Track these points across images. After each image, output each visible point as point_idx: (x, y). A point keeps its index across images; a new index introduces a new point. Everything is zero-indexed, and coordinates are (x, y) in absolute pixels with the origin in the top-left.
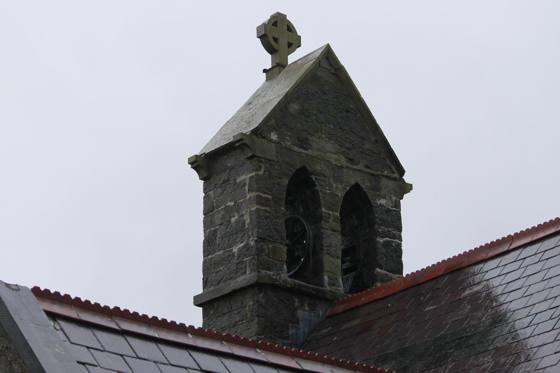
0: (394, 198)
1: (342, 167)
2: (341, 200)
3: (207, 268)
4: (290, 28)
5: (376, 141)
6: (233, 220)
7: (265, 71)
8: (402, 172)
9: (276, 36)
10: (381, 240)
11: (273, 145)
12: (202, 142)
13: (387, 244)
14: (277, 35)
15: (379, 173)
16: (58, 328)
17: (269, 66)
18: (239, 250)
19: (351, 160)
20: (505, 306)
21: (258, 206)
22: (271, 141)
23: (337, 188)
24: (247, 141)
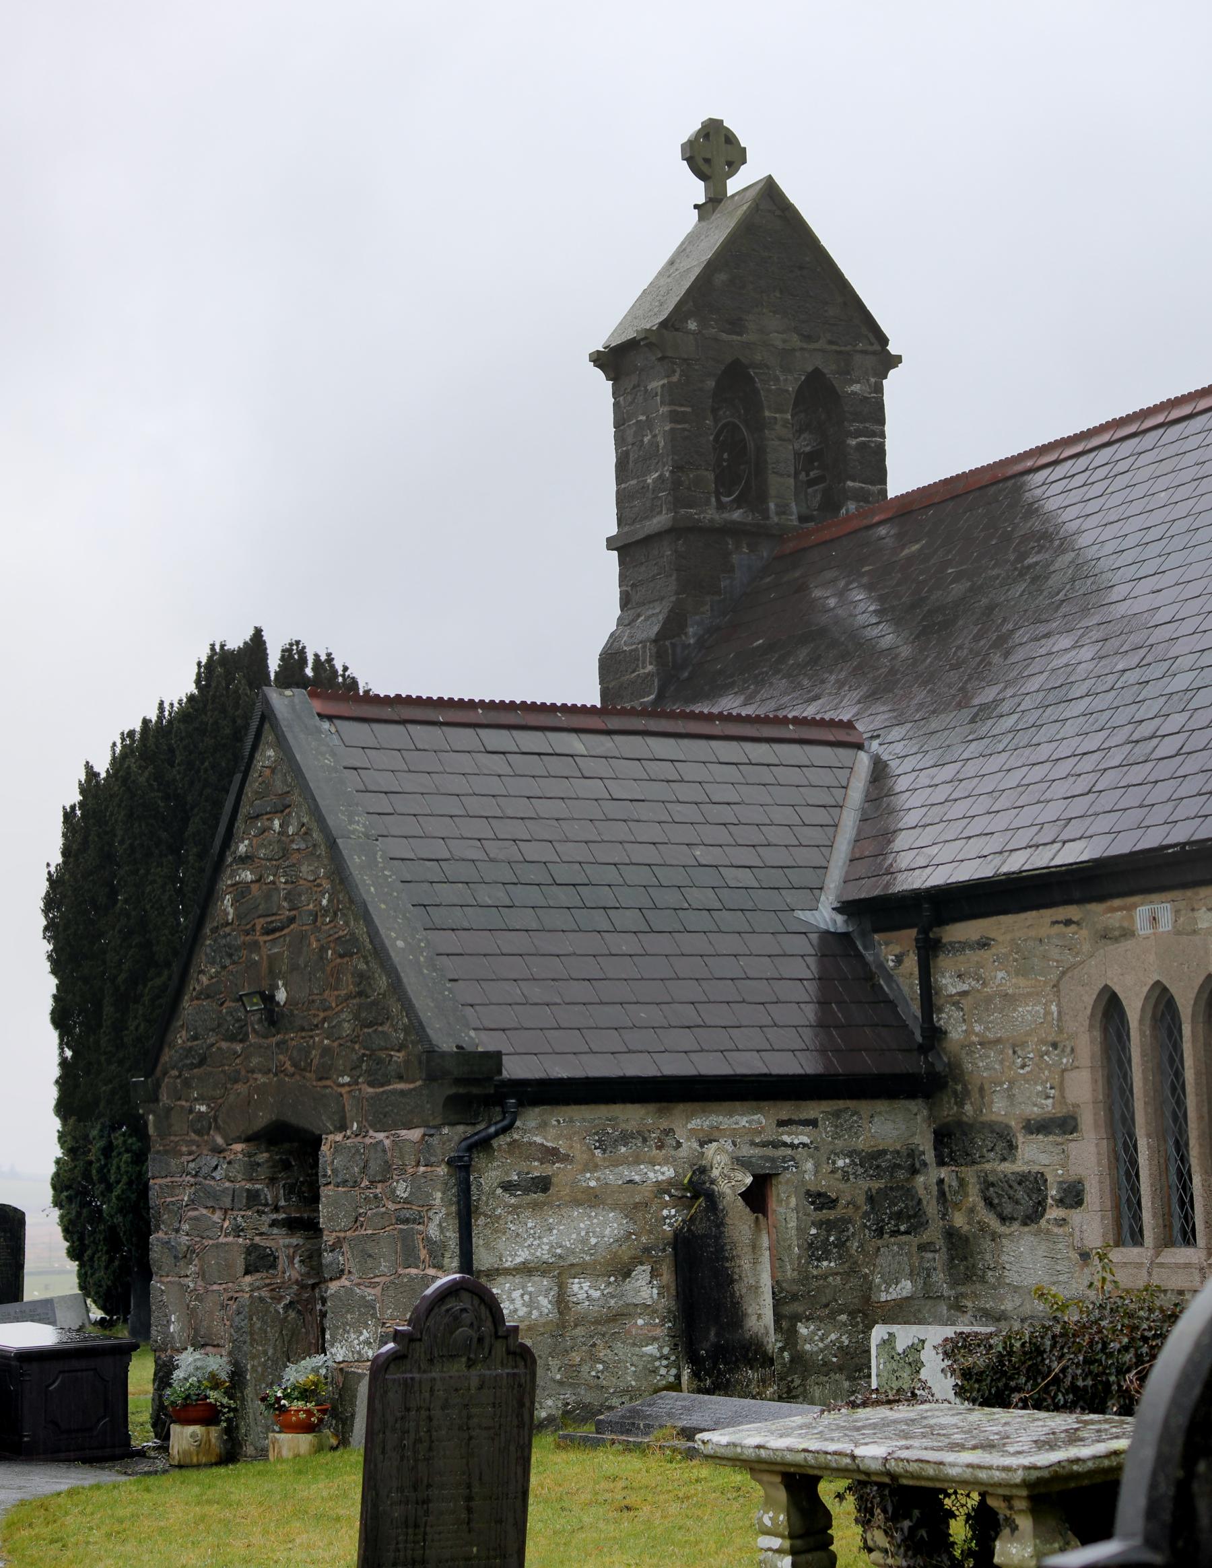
0: (873, 380)
1: (794, 350)
2: (793, 396)
3: (623, 499)
4: (730, 139)
5: (845, 304)
6: (646, 440)
7: (696, 207)
8: (883, 340)
9: (709, 156)
10: (853, 442)
11: (691, 337)
13: (863, 445)
14: (712, 151)
15: (849, 348)
16: (333, 730)
17: (701, 200)
18: (655, 481)
19: (808, 338)
21: (673, 425)
22: (689, 332)
23: (786, 380)
24: (653, 339)
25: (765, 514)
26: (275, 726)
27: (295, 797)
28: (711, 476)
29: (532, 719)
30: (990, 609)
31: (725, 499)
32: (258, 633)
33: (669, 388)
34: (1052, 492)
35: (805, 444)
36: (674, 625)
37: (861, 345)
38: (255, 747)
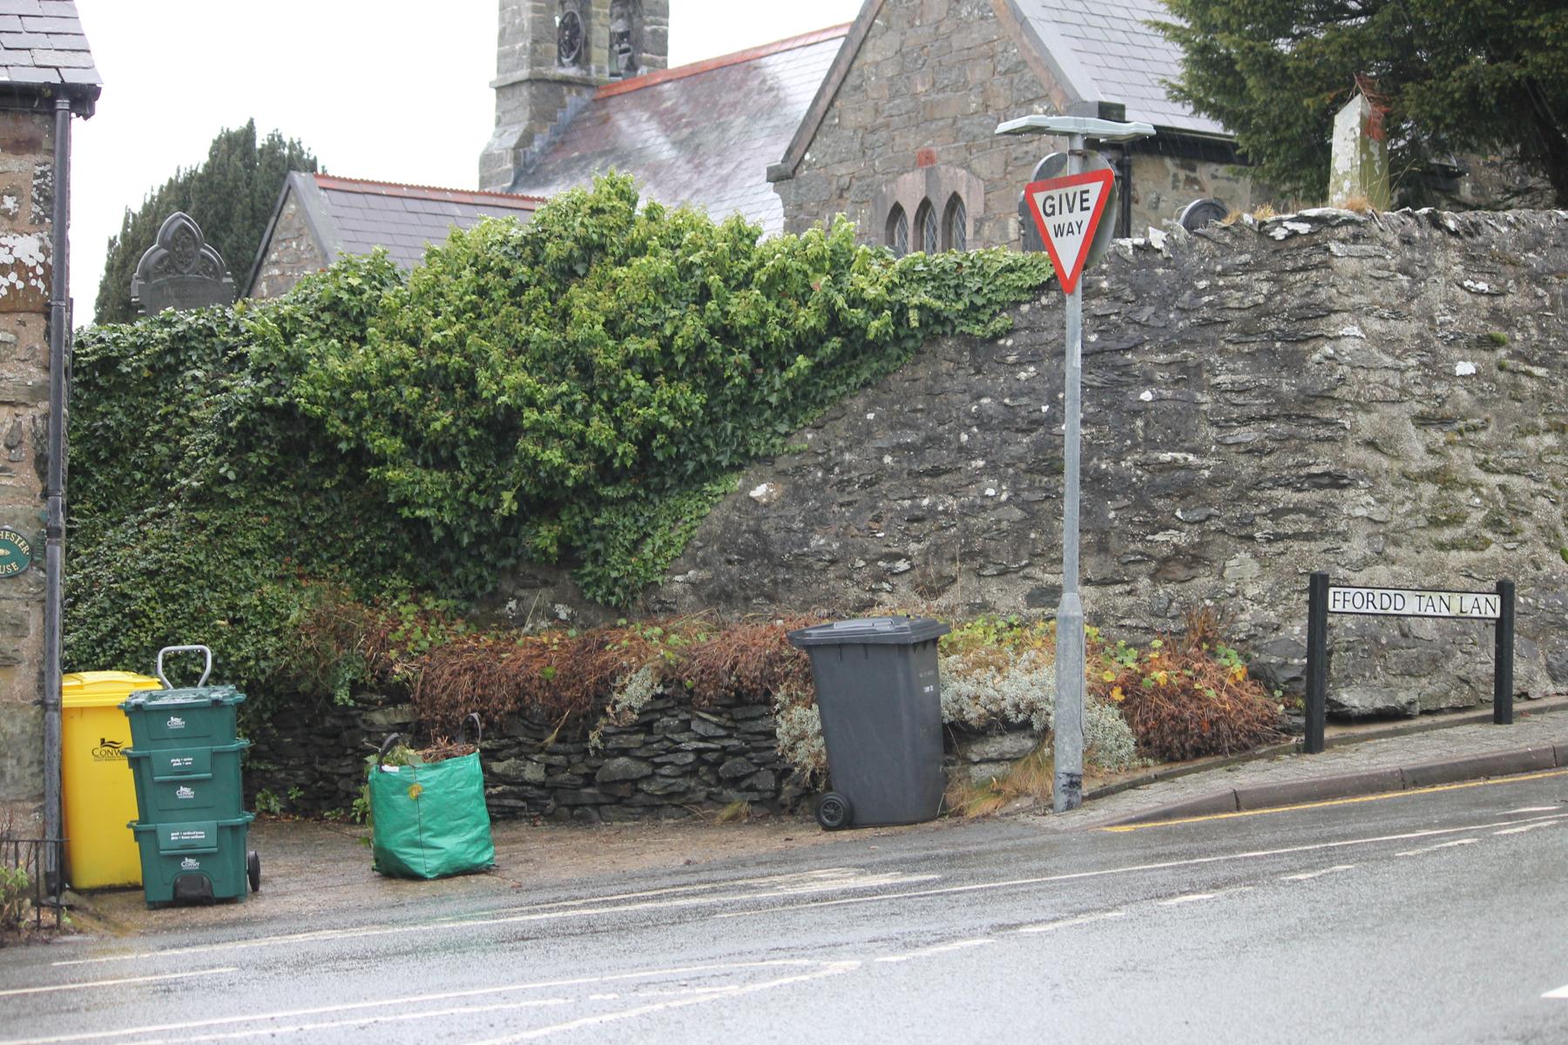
10: (648, 29)
13: (654, 32)
25: (589, 70)
27: (306, 230)
28: (555, 47)
30: (698, 146)
34: (776, 66)
35: (619, 26)
36: (527, 139)
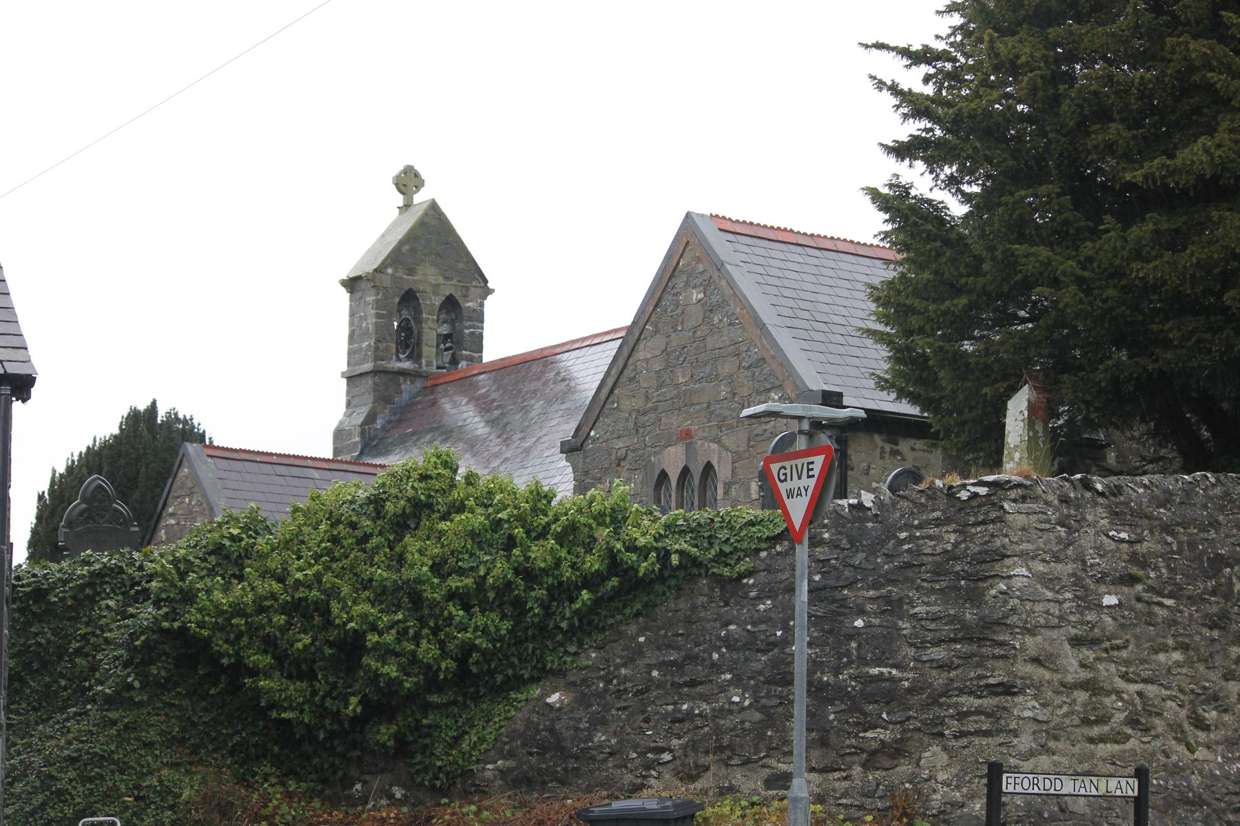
3: (351, 353)
4: (417, 175)
8: (486, 281)
10: (467, 331)
12: (345, 272)
13: (472, 333)
14: (408, 181)
19: (446, 278)
20: (899, 257)
25: (420, 364)
26: (189, 461)
28: (394, 346)
29: (297, 462)
31: (401, 356)
32: (154, 403)
33: (377, 301)
34: (569, 361)
35: (445, 329)
36: (371, 418)
37: (474, 280)
38: (179, 468)
